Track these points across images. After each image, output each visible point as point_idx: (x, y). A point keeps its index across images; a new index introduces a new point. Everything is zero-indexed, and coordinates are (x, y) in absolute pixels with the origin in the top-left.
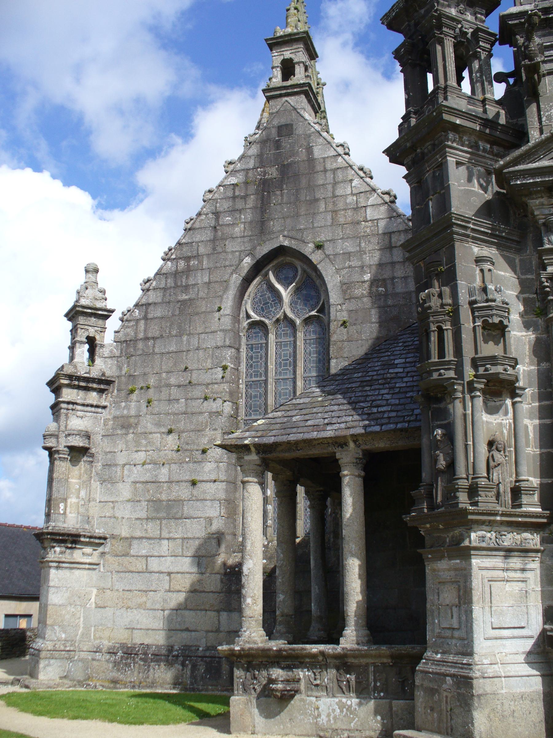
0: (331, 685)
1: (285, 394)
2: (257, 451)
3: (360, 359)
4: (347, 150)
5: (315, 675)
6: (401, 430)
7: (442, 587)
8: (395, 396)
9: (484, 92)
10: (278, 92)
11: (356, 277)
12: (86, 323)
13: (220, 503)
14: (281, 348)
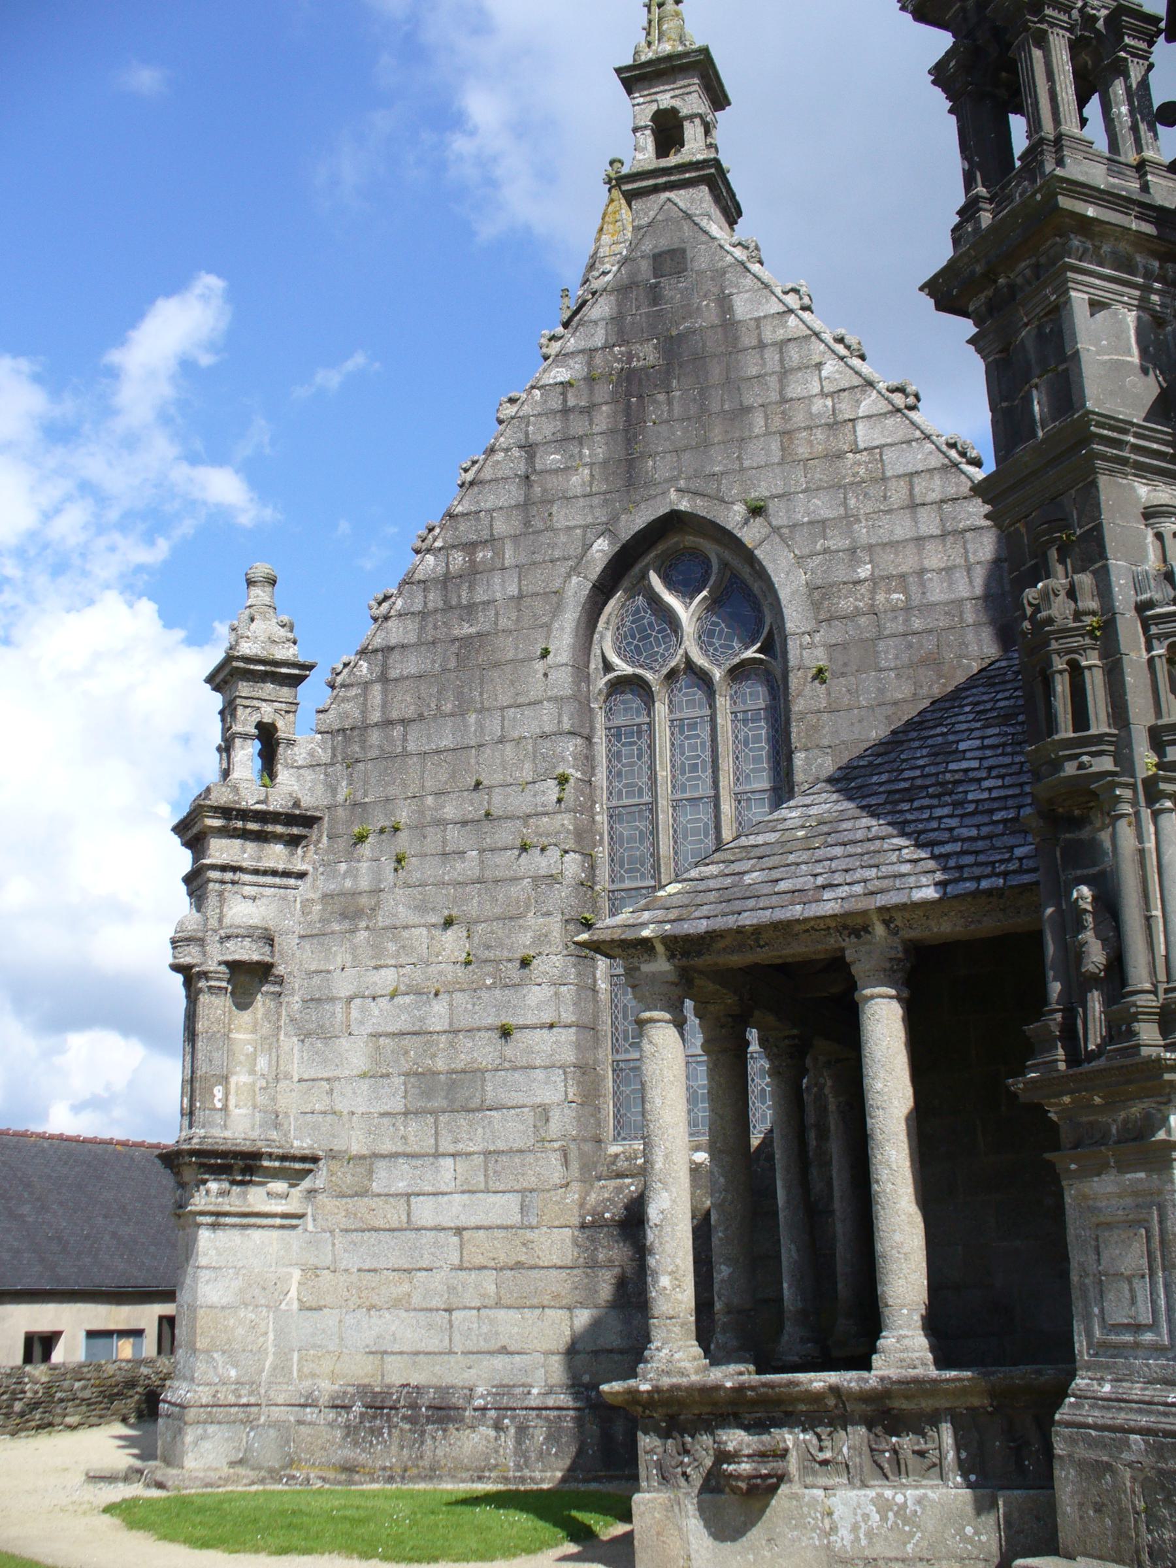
0: (858, 1460)
1: (695, 831)
2: (668, 953)
3: (881, 744)
4: (806, 300)
5: (820, 1440)
6: (989, 892)
7: (1106, 1234)
8: (968, 821)
9: (1139, 148)
10: (651, 182)
11: (840, 573)
12: (253, 694)
13: (565, 1073)
14: (682, 732)
